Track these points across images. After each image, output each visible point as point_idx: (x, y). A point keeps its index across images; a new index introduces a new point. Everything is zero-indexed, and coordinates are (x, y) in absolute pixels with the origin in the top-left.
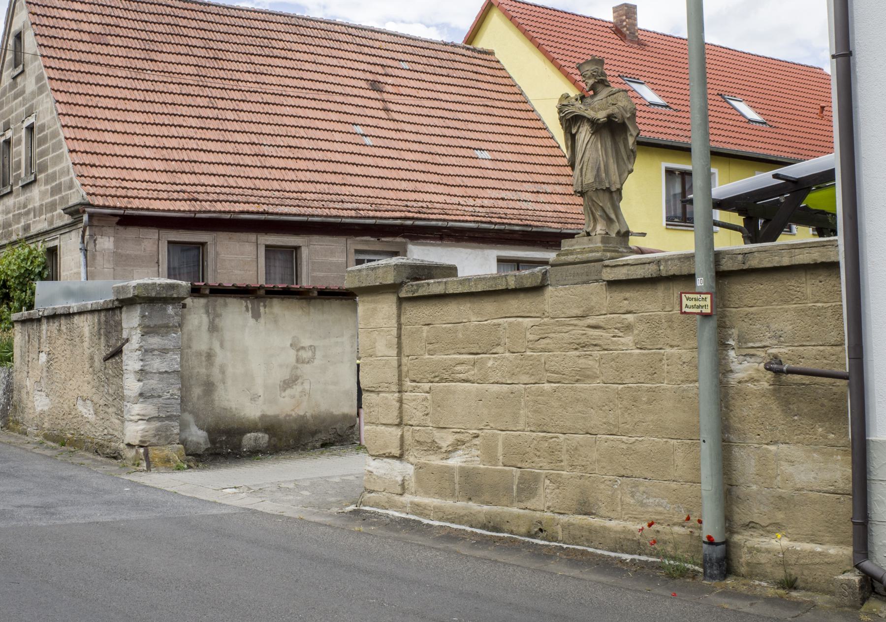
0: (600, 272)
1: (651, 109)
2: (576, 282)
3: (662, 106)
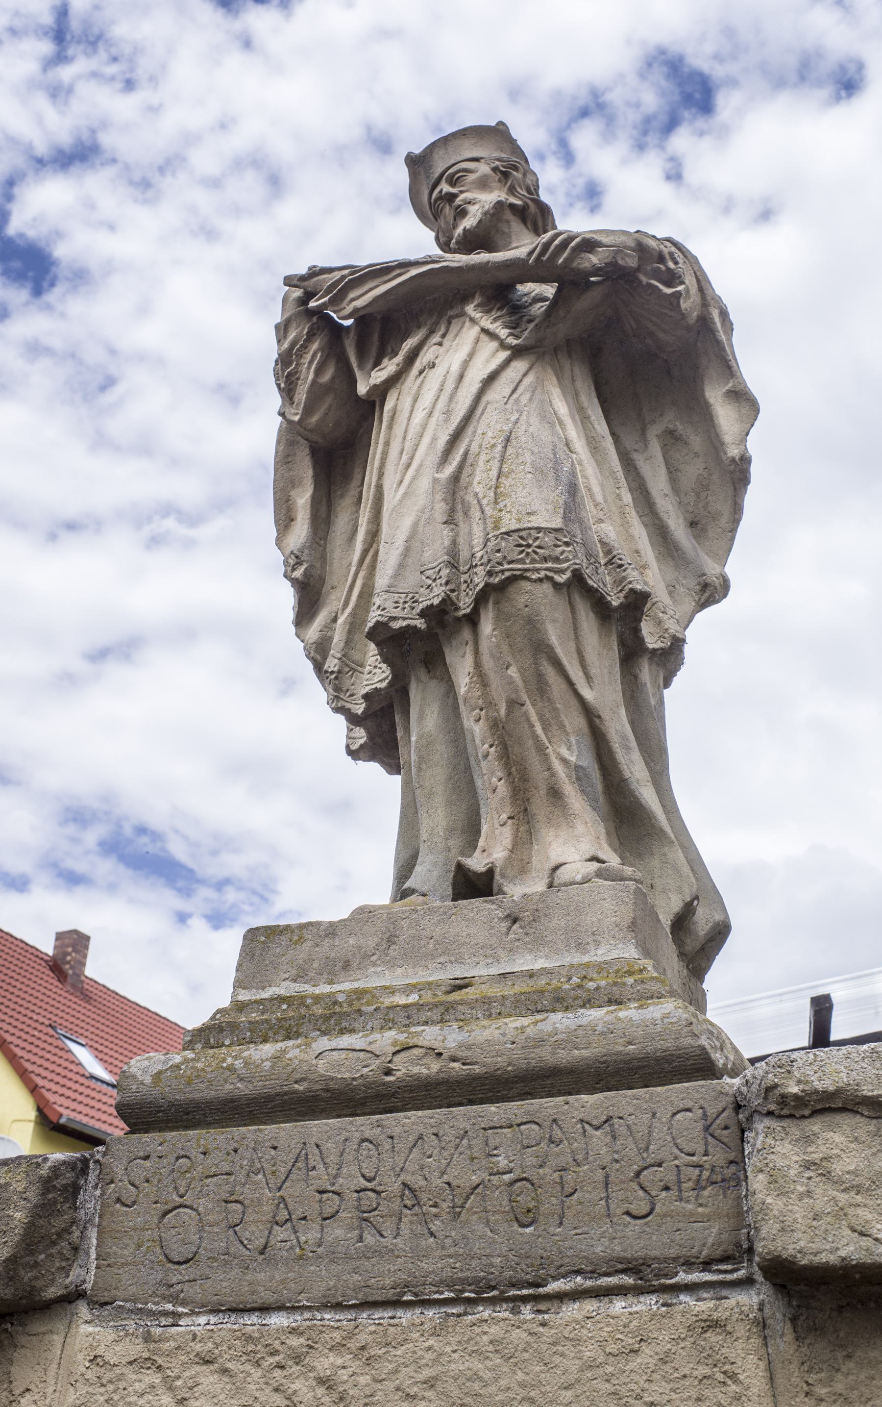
0: (733, 1175)
1: (92, 1084)
2: (385, 1276)
3: (108, 1084)
